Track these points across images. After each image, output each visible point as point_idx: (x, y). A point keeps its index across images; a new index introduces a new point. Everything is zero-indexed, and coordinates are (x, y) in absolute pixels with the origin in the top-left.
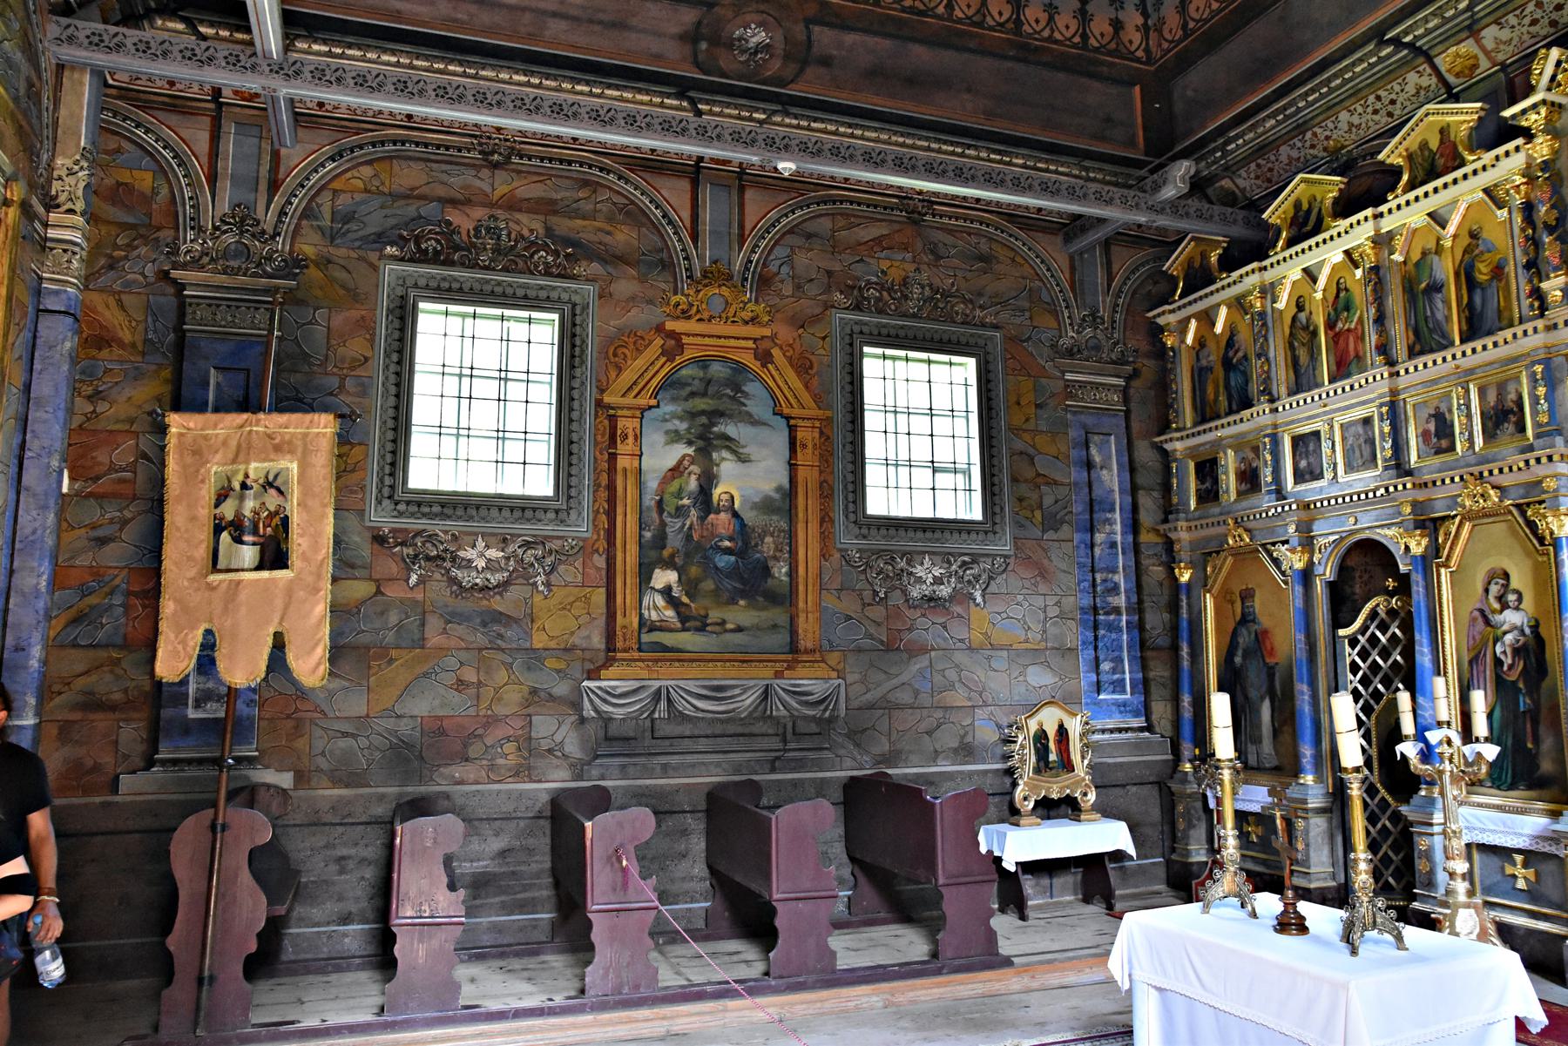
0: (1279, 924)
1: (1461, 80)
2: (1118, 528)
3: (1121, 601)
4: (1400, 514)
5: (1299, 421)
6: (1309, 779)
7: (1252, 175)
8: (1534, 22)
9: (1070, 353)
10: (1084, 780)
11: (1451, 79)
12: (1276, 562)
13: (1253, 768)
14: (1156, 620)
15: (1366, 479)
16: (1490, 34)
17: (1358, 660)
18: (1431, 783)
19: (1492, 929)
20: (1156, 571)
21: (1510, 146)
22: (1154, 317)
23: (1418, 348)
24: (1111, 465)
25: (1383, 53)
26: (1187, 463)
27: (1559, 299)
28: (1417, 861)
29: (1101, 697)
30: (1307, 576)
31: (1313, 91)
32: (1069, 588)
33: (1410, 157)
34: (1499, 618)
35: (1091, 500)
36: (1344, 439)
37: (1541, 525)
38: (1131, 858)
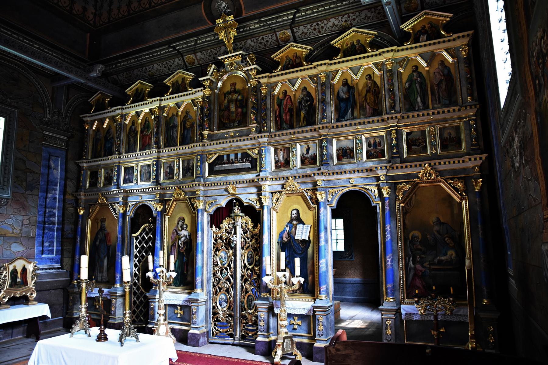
0: (98, 338)
1: (190, 65)
2: (58, 192)
3: (56, 220)
4: (155, 197)
5: (127, 162)
6: (118, 285)
7: (124, 76)
8: (210, 56)
9: (47, 124)
10: (32, 288)
11: (187, 64)
12: (114, 210)
13: (99, 282)
14: (68, 228)
15: (146, 185)
16: (199, 54)
17: (138, 245)
18: (156, 285)
19: (169, 330)
20: (71, 209)
21: (200, 89)
22: (83, 117)
23: (167, 144)
24: (58, 169)
25: (170, 50)
27: (206, 137)
28: (150, 311)
29: (43, 256)
30: (124, 215)
31: (147, 55)
32: (34, 213)
33: (173, 84)
34: (180, 232)
35: (48, 181)
36: (141, 170)
37: (195, 205)
38: (49, 318)
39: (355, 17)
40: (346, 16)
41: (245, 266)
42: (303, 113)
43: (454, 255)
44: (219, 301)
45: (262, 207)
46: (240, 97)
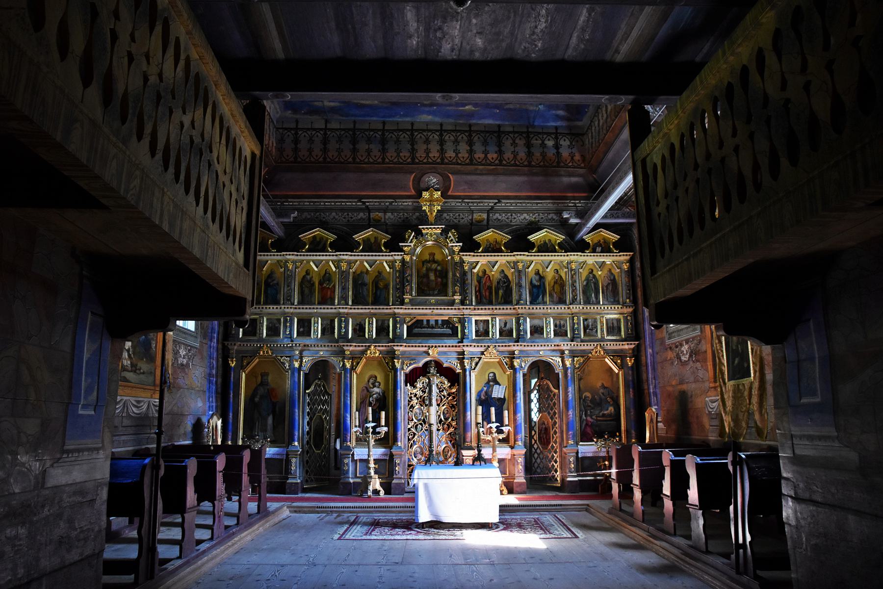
11: (372, 220)
16: (389, 215)
26: (294, 319)
39: (543, 217)
40: (537, 214)
41: (441, 421)
42: (501, 292)
43: (613, 410)
44: (414, 453)
45: (464, 370)
46: (439, 268)
